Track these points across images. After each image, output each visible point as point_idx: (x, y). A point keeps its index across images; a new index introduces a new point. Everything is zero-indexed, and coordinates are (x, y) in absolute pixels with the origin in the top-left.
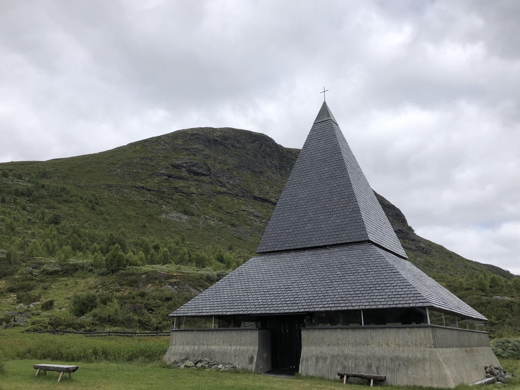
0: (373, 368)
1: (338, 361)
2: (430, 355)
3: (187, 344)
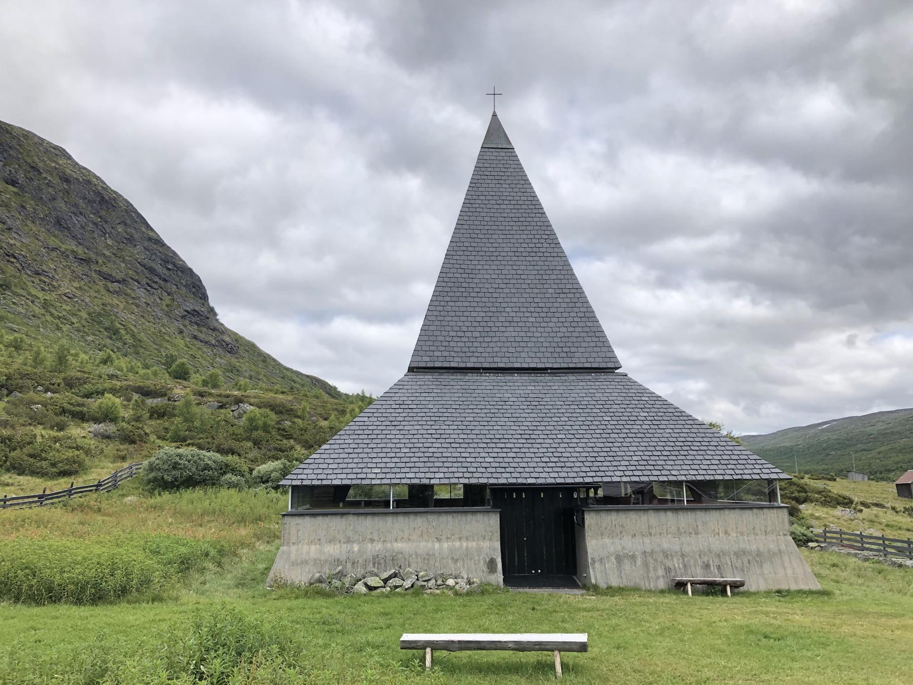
0: (712, 569)
1: (656, 560)
2: (787, 547)
3: (331, 541)
